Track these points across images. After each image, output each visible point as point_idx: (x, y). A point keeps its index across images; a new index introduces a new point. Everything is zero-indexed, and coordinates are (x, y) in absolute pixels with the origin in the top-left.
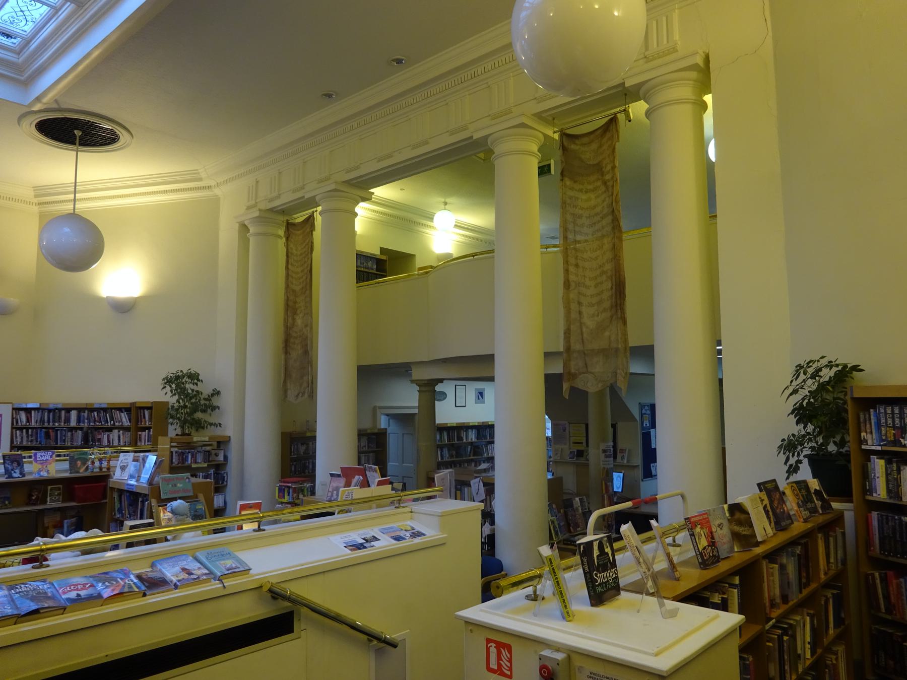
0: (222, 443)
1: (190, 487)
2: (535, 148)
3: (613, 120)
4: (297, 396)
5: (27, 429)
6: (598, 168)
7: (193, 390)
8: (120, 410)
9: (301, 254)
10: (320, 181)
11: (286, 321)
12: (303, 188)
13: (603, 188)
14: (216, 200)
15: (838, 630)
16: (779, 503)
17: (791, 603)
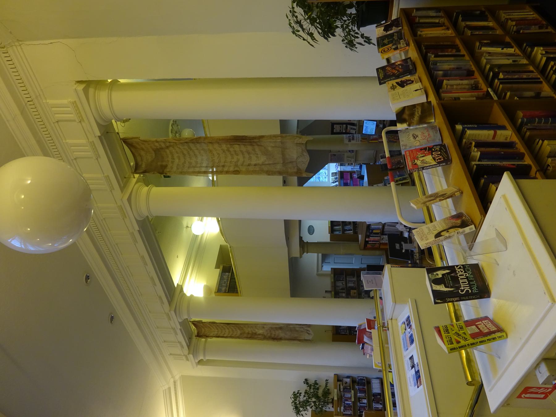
2: (145, 189)
3: (125, 141)
4: (309, 334)
6: (157, 151)
7: (304, 396)
9: (217, 329)
10: (169, 319)
11: (261, 339)
12: (174, 329)
13: (171, 148)
14: (183, 378)
15: (490, 18)
16: (394, 68)
17: (474, 68)
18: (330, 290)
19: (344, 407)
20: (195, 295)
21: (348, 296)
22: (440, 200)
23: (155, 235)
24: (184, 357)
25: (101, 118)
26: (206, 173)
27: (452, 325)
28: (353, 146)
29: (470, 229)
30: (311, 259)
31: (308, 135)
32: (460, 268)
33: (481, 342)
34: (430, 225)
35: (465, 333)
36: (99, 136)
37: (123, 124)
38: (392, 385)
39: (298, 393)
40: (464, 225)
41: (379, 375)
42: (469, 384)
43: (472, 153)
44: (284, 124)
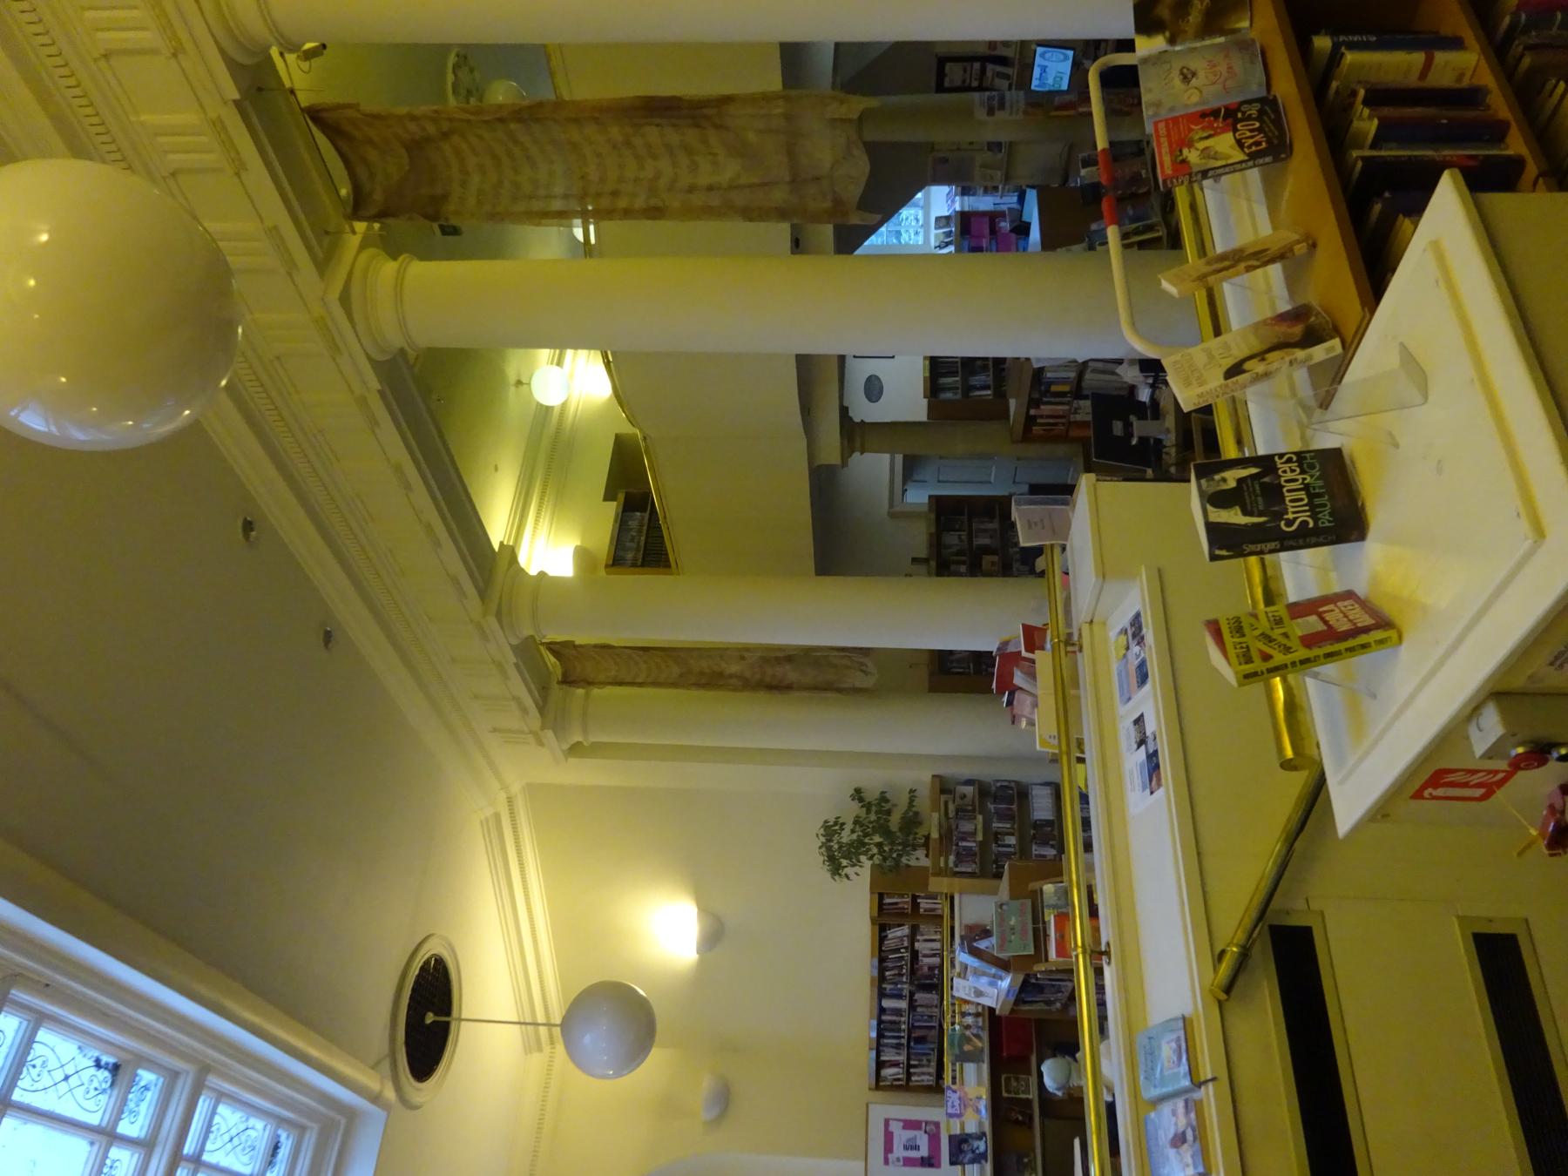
0: (944, 786)
1: (1017, 903)
2: (389, 267)
3: (316, 115)
5: (909, 1066)
6: (416, 147)
7: (853, 831)
8: (882, 939)
10: (484, 636)
11: (735, 689)
13: (455, 139)
18: (923, 554)
19: (958, 855)
20: (553, 572)
21: (975, 569)
22: (1249, 269)
24: (531, 739)
25: (229, 30)
26: (563, 216)
27: (1255, 616)
28: (1002, 127)
30: (874, 469)
31: (864, 95)
32: (1289, 460)
33: (1329, 656)
34: (1214, 343)
35: (1286, 635)
36: (235, 101)
37: (305, 65)
38: (1084, 798)
39: (836, 823)
40: (1311, 338)
41: (1049, 774)
42: (1287, 765)
43: (1356, 124)
44: (793, 56)
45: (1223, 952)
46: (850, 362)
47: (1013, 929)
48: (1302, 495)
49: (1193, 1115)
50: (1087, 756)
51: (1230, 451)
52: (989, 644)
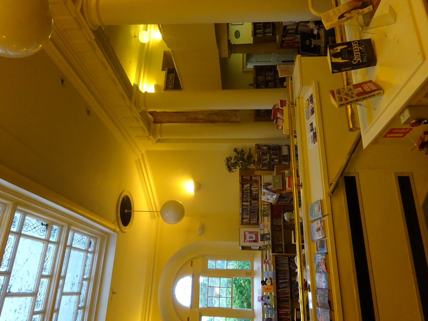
0: (258, 147)
4: (237, 117)
5: (250, 219)
7: (234, 160)
10: (131, 110)
19: (262, 165)
20: (149, 91)
23: (110, 45)
24: (146, 138)
27: (344, 89)
29: (369, 9)
30: (238, 58)
32: (356, 43)
33: (364, 98)
34: (336, 9)
35: (352, 93)
45: (332, 184)
46: (231, 27)
47: (277, 182)
48: (359, 53)
49: (322, 224)
50: (297, 135)
51: (339, 41)
52: (271, 108)
